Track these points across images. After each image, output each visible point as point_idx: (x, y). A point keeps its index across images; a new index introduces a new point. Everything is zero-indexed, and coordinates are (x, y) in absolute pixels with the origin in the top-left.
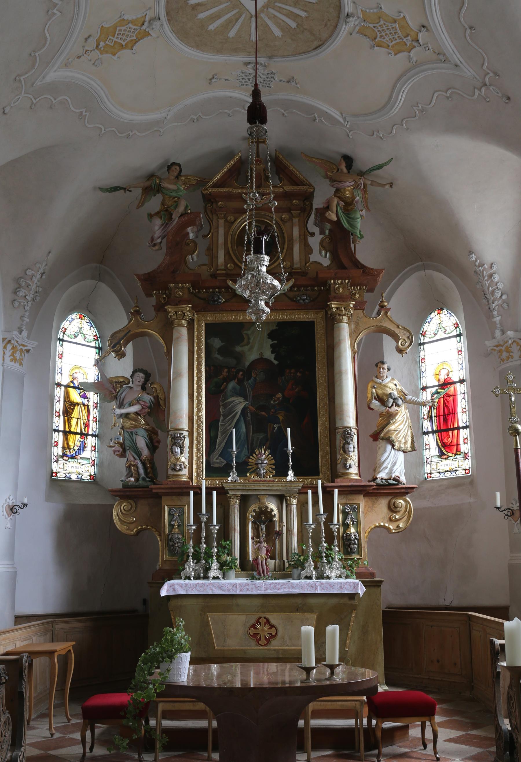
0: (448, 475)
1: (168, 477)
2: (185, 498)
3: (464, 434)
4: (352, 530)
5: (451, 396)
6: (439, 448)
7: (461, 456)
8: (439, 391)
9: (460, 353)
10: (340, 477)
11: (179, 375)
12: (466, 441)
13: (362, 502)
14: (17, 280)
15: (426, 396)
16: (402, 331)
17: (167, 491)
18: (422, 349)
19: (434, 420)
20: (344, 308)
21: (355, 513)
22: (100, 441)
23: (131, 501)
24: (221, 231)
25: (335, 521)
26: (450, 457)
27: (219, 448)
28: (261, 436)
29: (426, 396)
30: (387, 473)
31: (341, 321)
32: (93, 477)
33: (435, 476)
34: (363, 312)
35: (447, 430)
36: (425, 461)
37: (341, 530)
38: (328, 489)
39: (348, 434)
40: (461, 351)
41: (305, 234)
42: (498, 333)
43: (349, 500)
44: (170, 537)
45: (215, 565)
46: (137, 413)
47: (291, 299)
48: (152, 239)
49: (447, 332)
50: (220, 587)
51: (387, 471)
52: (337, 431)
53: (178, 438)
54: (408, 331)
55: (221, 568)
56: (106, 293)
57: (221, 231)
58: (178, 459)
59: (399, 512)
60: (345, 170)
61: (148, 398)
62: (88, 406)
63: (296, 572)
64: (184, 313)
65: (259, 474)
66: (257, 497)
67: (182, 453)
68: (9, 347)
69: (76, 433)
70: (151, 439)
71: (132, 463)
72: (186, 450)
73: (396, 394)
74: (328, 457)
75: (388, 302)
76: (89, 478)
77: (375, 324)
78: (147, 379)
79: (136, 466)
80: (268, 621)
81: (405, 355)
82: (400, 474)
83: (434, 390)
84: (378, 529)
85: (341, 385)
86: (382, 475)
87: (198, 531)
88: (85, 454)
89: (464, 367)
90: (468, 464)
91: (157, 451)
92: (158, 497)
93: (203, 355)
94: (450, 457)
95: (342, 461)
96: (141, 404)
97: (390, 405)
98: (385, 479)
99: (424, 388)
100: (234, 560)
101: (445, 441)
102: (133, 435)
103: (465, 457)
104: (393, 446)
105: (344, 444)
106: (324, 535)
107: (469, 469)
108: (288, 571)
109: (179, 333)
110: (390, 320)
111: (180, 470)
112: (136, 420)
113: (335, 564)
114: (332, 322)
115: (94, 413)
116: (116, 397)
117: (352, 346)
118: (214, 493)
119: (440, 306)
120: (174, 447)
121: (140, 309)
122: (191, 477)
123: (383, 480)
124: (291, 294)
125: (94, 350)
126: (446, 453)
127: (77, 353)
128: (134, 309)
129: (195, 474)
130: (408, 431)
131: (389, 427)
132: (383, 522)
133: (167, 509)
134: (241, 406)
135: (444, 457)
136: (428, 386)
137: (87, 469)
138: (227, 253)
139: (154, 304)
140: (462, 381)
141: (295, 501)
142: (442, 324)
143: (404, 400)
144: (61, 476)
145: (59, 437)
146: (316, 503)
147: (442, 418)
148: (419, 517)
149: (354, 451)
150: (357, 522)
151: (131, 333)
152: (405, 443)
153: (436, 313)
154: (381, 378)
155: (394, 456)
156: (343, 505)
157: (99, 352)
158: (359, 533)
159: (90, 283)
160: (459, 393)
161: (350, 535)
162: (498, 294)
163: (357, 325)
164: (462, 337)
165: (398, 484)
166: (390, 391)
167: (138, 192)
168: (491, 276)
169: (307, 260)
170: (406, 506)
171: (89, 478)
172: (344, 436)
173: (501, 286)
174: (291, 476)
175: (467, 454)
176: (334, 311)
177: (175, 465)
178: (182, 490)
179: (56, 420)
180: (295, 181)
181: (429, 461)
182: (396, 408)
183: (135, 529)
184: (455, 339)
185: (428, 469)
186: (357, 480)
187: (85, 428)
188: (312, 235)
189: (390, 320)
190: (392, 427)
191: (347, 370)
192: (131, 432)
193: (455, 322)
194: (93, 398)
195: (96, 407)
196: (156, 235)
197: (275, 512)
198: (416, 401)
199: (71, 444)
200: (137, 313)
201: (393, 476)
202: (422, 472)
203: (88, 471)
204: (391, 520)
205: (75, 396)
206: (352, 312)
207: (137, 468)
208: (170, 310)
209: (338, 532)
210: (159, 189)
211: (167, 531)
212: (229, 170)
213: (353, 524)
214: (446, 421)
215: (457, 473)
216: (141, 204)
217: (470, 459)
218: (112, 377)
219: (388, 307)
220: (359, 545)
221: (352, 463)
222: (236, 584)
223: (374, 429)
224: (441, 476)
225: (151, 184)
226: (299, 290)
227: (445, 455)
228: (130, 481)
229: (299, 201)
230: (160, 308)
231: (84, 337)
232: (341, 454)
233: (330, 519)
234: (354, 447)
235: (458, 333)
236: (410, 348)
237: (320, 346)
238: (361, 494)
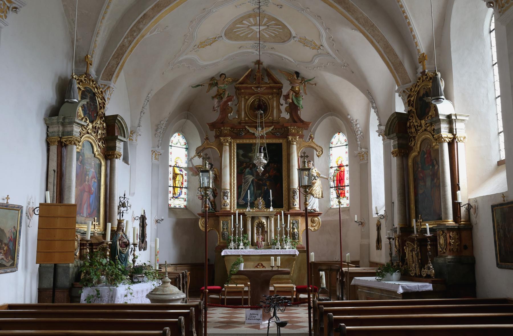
1: (221, 208)
2: (229, 218)
4: (296, 230)
11: (226, 166)
14: (157, 126)
15: (332, 171)
19: (335, 182)
24: (243, 103)
27: (242, 196)
28: (260, 191)
31: (293, 144)
32: (185, 206)
41: (279, 104)
42: (359, 148)
45: (242, 244)
47: (273, 134)
48: (214, 108)
50: (244, 252)
55: (244, 245)
56: (191, 126)
57: (243, 103)
58: (226, 202)
60: (296, 78)
63: (273, 246)
65: (258, 208)
66: (258, 217)
68: (154, 154)
69: (178, 187)
70: (214, 193)
72: (229, 197)
73: (315, 175)
74: (287, 200)
80: (262, 265)
85: (292, 172)
87: (235, 231)
88: (181, 196)
90: (348, 202)
92: (218, 217)
93: (236, 157)
99: (331, 168)
100: (249, 242)
108: (270, 246)
113: (288, 244)
114: (289, 144)
115: (185, 178)
117: (298, 154)
118: (241, 216)
122: (231, 209)
124: (273, 131)
127: (179, 151)
129: (232, 207)
133: (221, 222)
134: (252, 179)
138: (245, 113)
140: (347, 166)
141: (273, 219)
142: (340, 139)
144: (172, 206)
145: (171, 189)
146: (281, 220)
156: (292, 220)
158: (298, 231)
159: (183, 120)
162: (359, 133)
167: (207, 86)
168: (356, 125)
169: (279, 117)
173: (360, 129)
174: (271, 209)
178: (228, 214)
179: (170, 181)
180: (275, 82)
188: (282, 105)
194: (184, 172)
196: (216, 106)
197: (265, 223)
199: (176, 192)
200: (207, 139)
205: (177, 171)
210: (216, 84)
211: (221, 230)
212: (246, 76)
214: (340, 182)
216: (208, 91)
220: (298, 236)
222: (250, 251)
225: (213, 82)
226: (276, 130)
229: (276, 89)
230: (217, 137)
233: (286, 226)
237: (284, 153)
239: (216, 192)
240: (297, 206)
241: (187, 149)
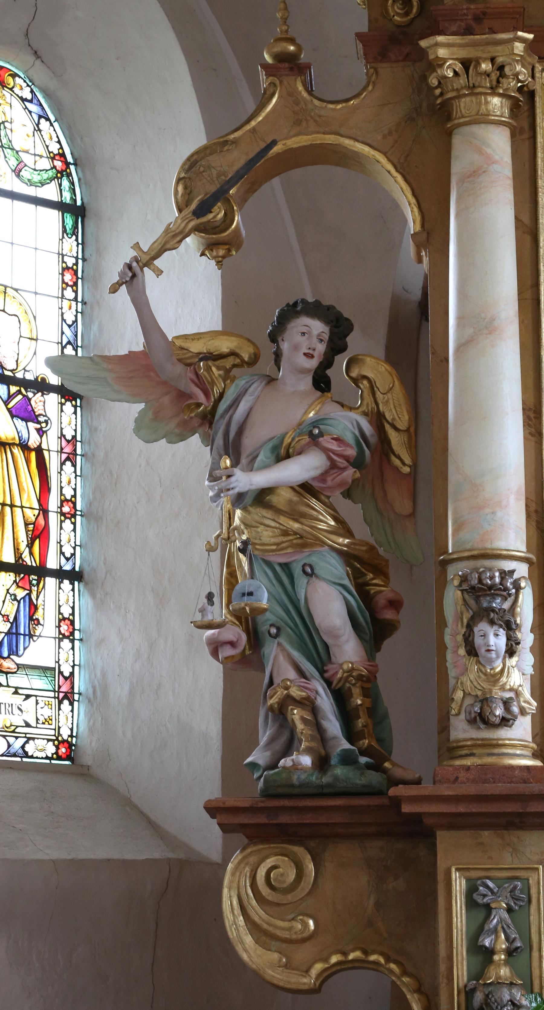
1: (449, 750)
11: (480, 327)
17: (461, 808)
22: (93, 595)
23: (299, 850)
32: (68, 749)
44: (479, 997)
46: (306, 488)
53: (493, 591)
61: (347, 424)
62: (39, 451)
64: (501, 68)
67: (511, 652)
71: (295, 692)
76: (51, 749)
78: (336, 345)
79: (308, 703)
91: (387, 644)
96: (326, 451)
102: (291, 577)
109: (480, 152)
111: (505, 722)
112: (304, 515)
116: (208, 418)
120: (482, 627)
121: (299, 48)
125: (55, 214)
128: (278, 48)
133: (459, 884)
137: (46, 712)
139: (364, 28)
151: (277, 149)
157: (75, 227)
171: (51, 749)
177: (485, 701)
183: (319, 967)
187: (30, 546)
192: (286, 566)
193: (54, 148)
195: (71, 458)
203: (48, 721)
207: (314, 710)
208: (442, 52)
211: (461, 972)
218: (185, 337)
228: (296, 767)
231: (13, 163)
239: (382, 590)
241: (76, 212)
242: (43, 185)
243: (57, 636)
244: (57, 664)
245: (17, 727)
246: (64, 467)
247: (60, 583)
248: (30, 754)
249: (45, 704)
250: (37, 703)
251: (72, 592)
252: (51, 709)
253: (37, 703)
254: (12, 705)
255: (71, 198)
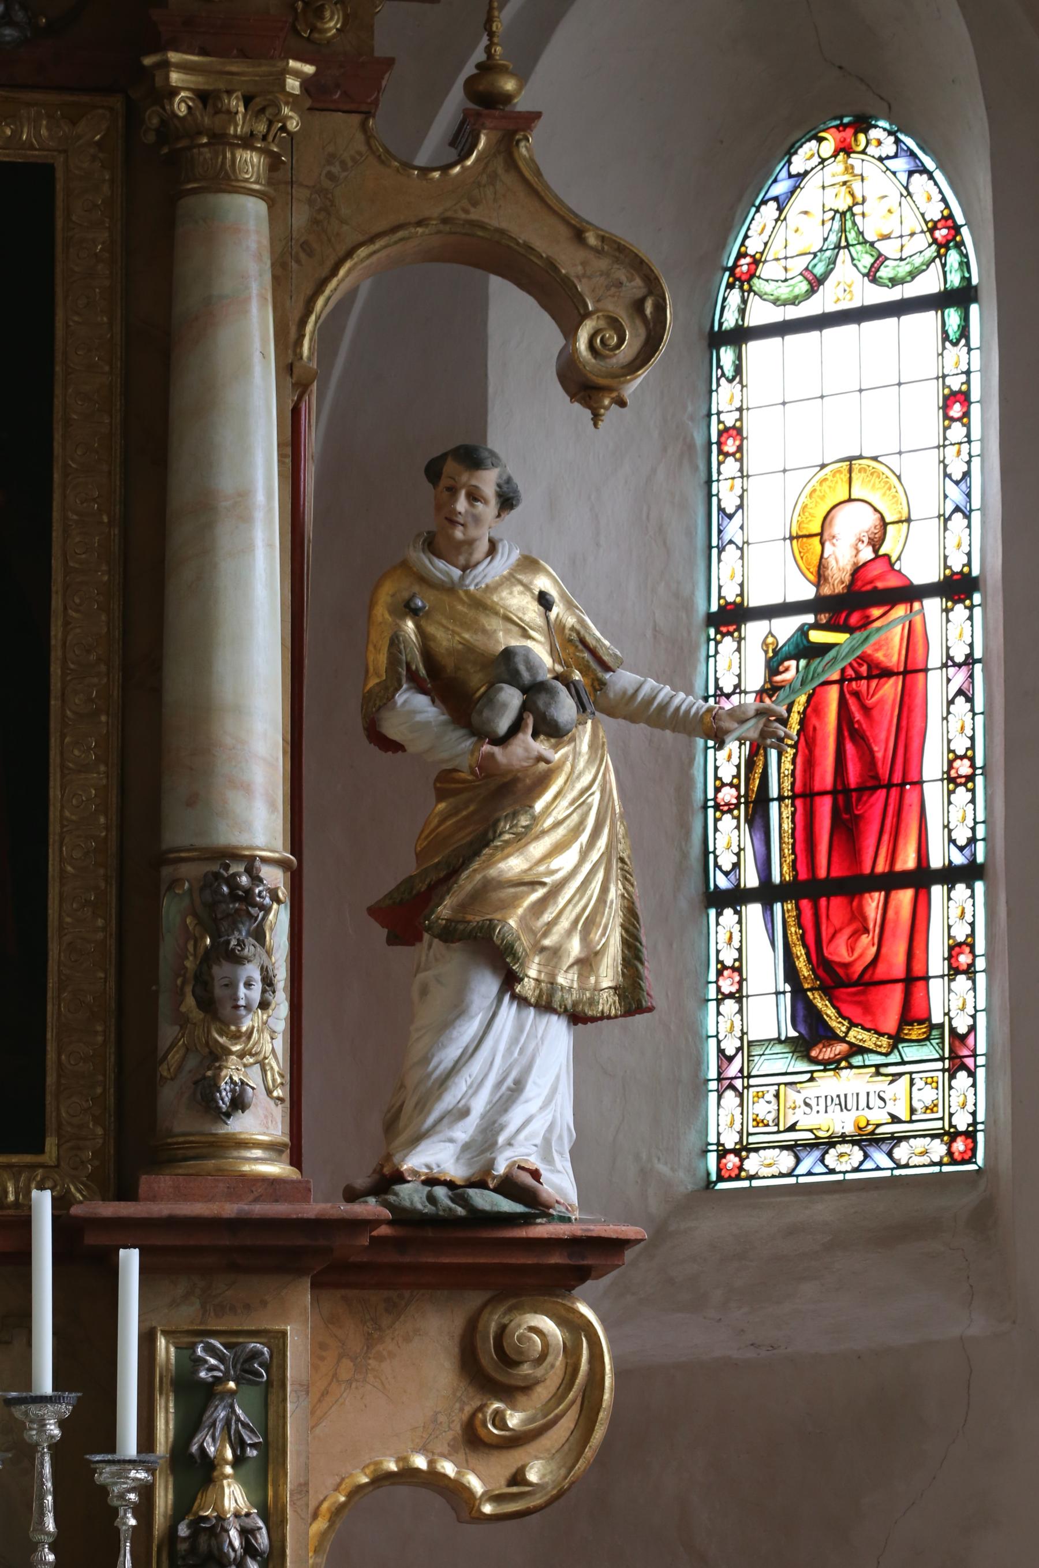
0: (845, 1161)
3: (956, 913)
4: (234, 1497)
5: (886, 673)
6: (798, 993)
7: (928, 1051)
8: (817, 637)
9: (956, 410)
10: (518, 565)
12: (964, 959)
13: (297, 1327)
15: (739, 665)
16: (603, 264)
18: (729, 370)
20: (247, 100)
21: (253, 1394)
25: (129, 1444)
26: (862, 1050)
29: (739, 665)
30: (466, 1147)
31: (226, 181)
33: (768, 1166)
34: (364, 126)
35: (855, 886)
36: (713, 1073)
37: (163, 1500)
38: (91, 1239)
39: (233, 897)
40: (963, 397)
43: (221, 1310)
49: (884, 273)
51: (464, 1131)
52: (167, 871)
54: (639, 265)
59: (527, 1388)
75: (523, 80)
77: (436, 211)
81: (612, 414)
82: (547, 1157)
83: (785, 628)
84: (403, 1491)
86: (438, 1156)
89: (976, 503)
90: (967, 1099)
94: (862, 1050)
95: (192, 1063)
97: (503, 725)
98: (450, 1185)
99: (732, 617)
101: (839, 951)
103: (954, 1056)
104: (510, 980)
105: (209, 958)
106: (50, 1525)
107: (970, 1135)
110: (533, 192)
114: (165, 182)
117: (287, 340)
119: (849, 93)
123: (441, 1192)
126: (839, 1026)
130: (604, 889)
131: (490, 862)
132: (423, 1450)
135: (828, 1053)
136: (754, 601)
137: (925, 1095)
140: (956, 587)
143: (594, 697)
147: (825, 807)
148: (643, 1426)
149: (264, 1005)
150: (263, 1448)
152: (587, 963)
153: (828, 148)
154: (458, 551)
155: (514, 1040)
158: (272, 1514)
160: (935, 659)
161: (217, 1528)
163: (324, 207)
164: (974, 309)
165: (526, 1220)
166: (506, 639)
170: (571, 1352)
172: (212, 906)
175: (963, 1038)
176: (182, 110)
181: (733, 1070)
182: (541, 747)
184: (929, 319)
185: (723, 1119)
186: (272, 1182)
189: (533, 192)
190: (514, 865)
191: (244, 495)
193: (935, 212)
198: (663, 707)
201: (501, 1168)
202: (692, 1140)
204: (474, 1441)
206: (293, 125)
209: (145, 1509)
213: (238, 1462)
214: (847, 828)
215: (902, 1152)
217: (981, 1073)
219: (522, 104)
221: (253, 1078)
223: (396, 867)
224: (802, 1169)
227: (833, 1037)
232: (183, 1021)
233: (93, 1424)
234: (268, 982)
235: (955, 280)
236: (643, 374)
237: (82, 328)
238: (299, 1272)
240: (261, 1123)
242: (913, 278)
243: (946, 972)
244: (947, 1017)
245: (878, 1126)
246: (952, 708)
247: (949, 891)
248: (903, 1162)
249: (926, 1083)
250: (912, 1084)
251: (738, 926)
252: (937, 1088)
253: (912, 1084)
254: (858, 1094)
255: (963, 278)
